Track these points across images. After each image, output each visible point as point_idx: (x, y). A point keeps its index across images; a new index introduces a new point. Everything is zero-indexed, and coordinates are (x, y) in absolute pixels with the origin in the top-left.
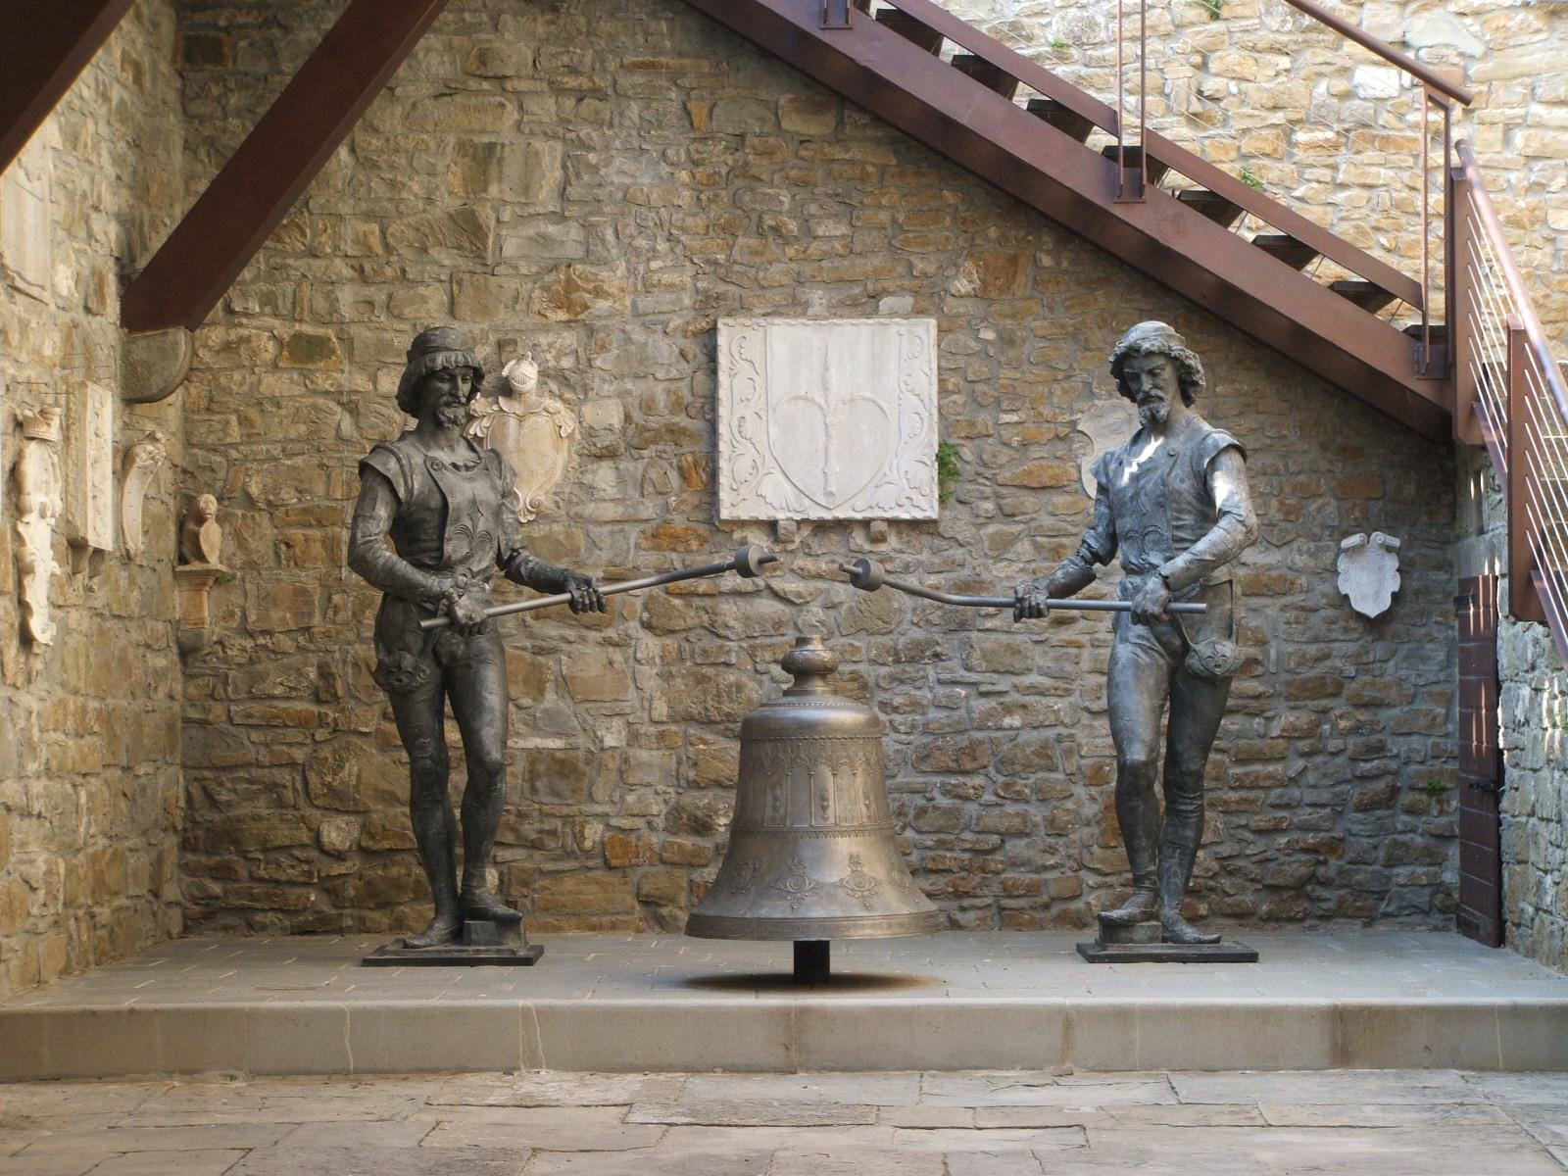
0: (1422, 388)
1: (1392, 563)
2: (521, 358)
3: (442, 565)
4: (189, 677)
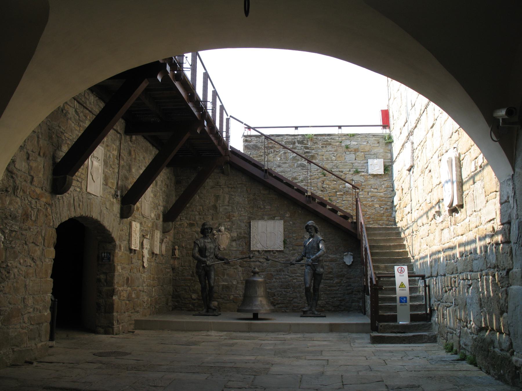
0: (353, 231)
1: (352, 257)
2: (222, 226)
3: (206, 257)
4: (173, 273)
